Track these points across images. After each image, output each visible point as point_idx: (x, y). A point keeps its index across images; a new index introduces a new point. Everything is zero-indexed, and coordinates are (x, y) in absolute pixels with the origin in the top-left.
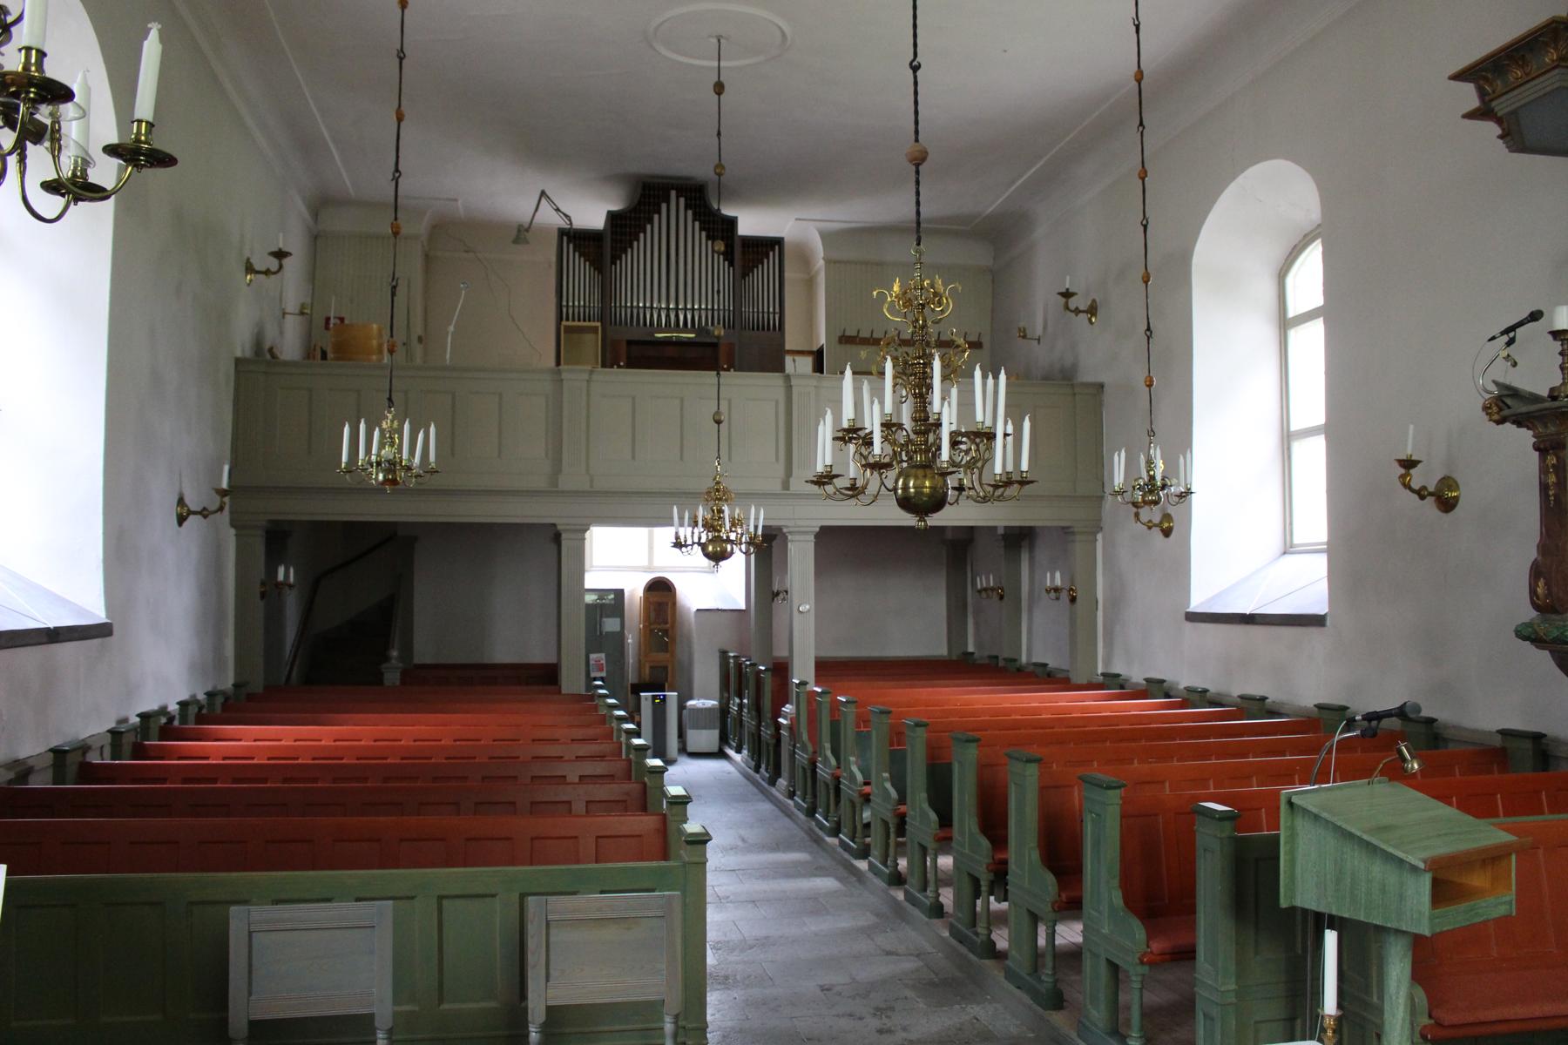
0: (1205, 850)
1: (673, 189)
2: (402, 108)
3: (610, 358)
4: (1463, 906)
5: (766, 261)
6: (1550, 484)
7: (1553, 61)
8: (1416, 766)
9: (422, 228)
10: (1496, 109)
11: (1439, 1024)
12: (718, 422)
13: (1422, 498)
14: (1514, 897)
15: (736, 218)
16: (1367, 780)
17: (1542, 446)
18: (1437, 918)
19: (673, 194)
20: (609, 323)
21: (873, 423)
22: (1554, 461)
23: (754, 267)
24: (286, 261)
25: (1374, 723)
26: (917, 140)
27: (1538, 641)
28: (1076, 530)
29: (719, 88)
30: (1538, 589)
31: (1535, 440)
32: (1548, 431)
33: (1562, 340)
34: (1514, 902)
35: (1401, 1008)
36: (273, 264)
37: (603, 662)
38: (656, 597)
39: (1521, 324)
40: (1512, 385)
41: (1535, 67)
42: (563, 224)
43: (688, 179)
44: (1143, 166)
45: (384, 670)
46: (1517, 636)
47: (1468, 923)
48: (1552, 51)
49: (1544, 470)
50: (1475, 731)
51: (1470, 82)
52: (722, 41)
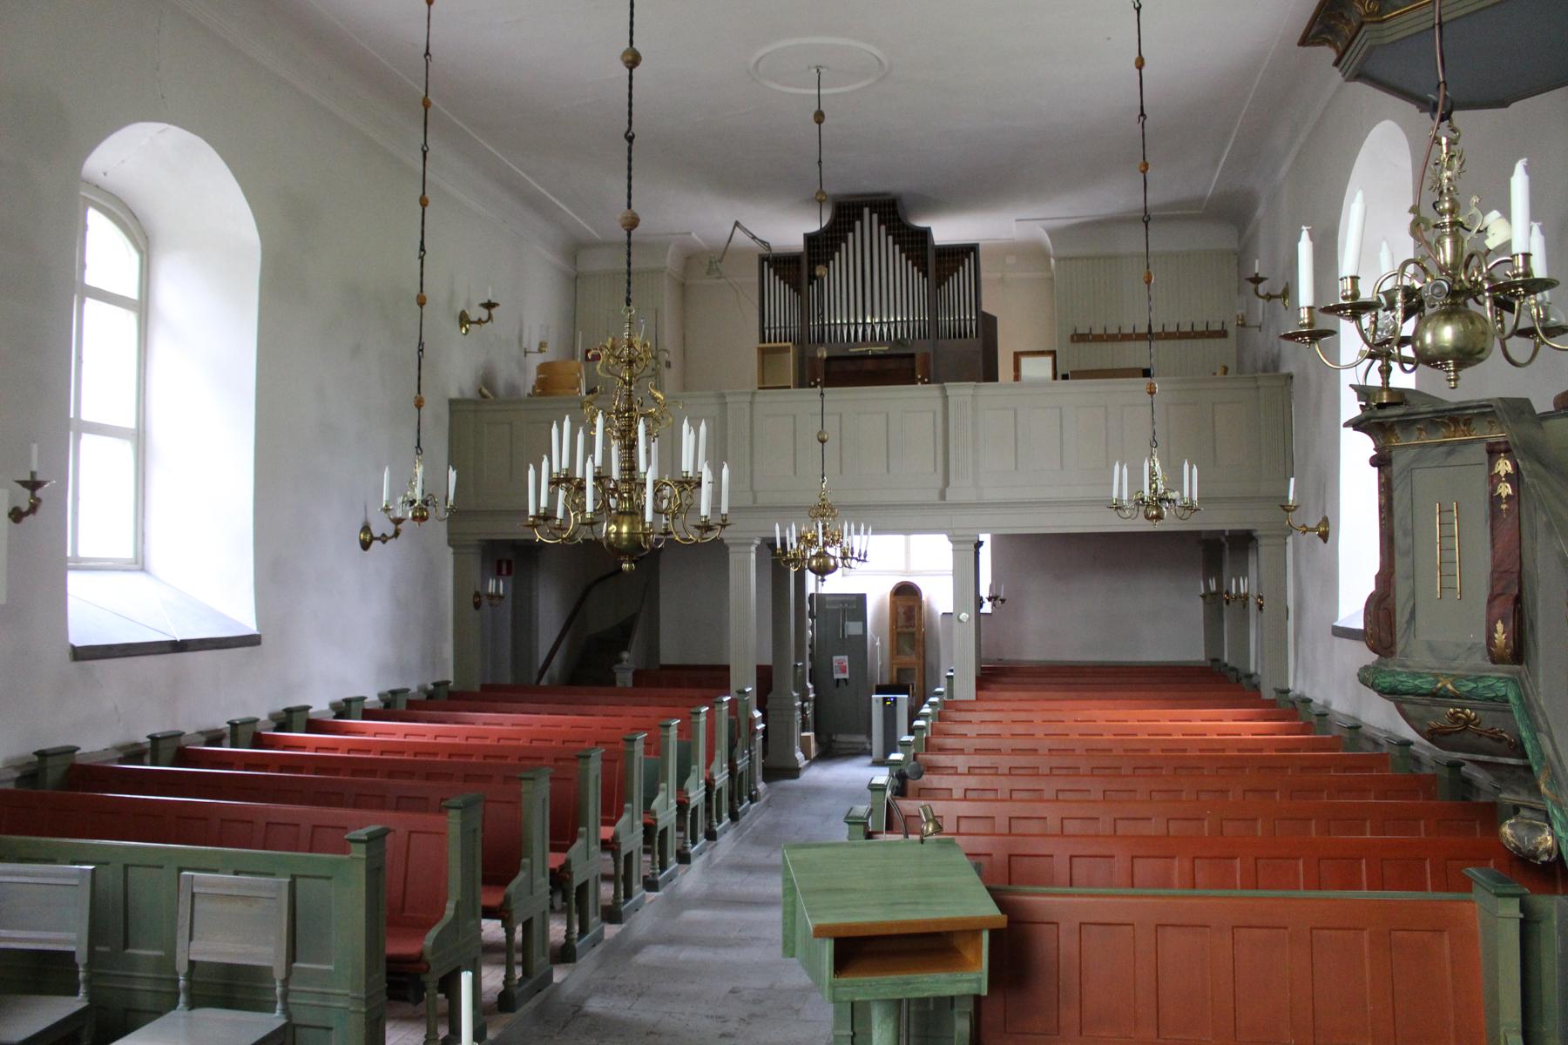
1: (866, 206)
2: (427, 195)
3: (804, 380)
5: (961, 268)
9: (670, 261)
12: (823, 441)
15: (929, 228)
19: (866, 211)
20: (807, 342)
21: (587, 471)
22: (1509, 468)
23: (949, 275)
24: (494, 311)
26: (629, 206)
28: (1258, 533)
29: (819, 117)
36: (484, 314)
37: (846, 664)
38: (903, 602)
42: (764, 252)
43: (884, 194)
44: (1144, 158)
45: (615, 671)
52: (821, 70)
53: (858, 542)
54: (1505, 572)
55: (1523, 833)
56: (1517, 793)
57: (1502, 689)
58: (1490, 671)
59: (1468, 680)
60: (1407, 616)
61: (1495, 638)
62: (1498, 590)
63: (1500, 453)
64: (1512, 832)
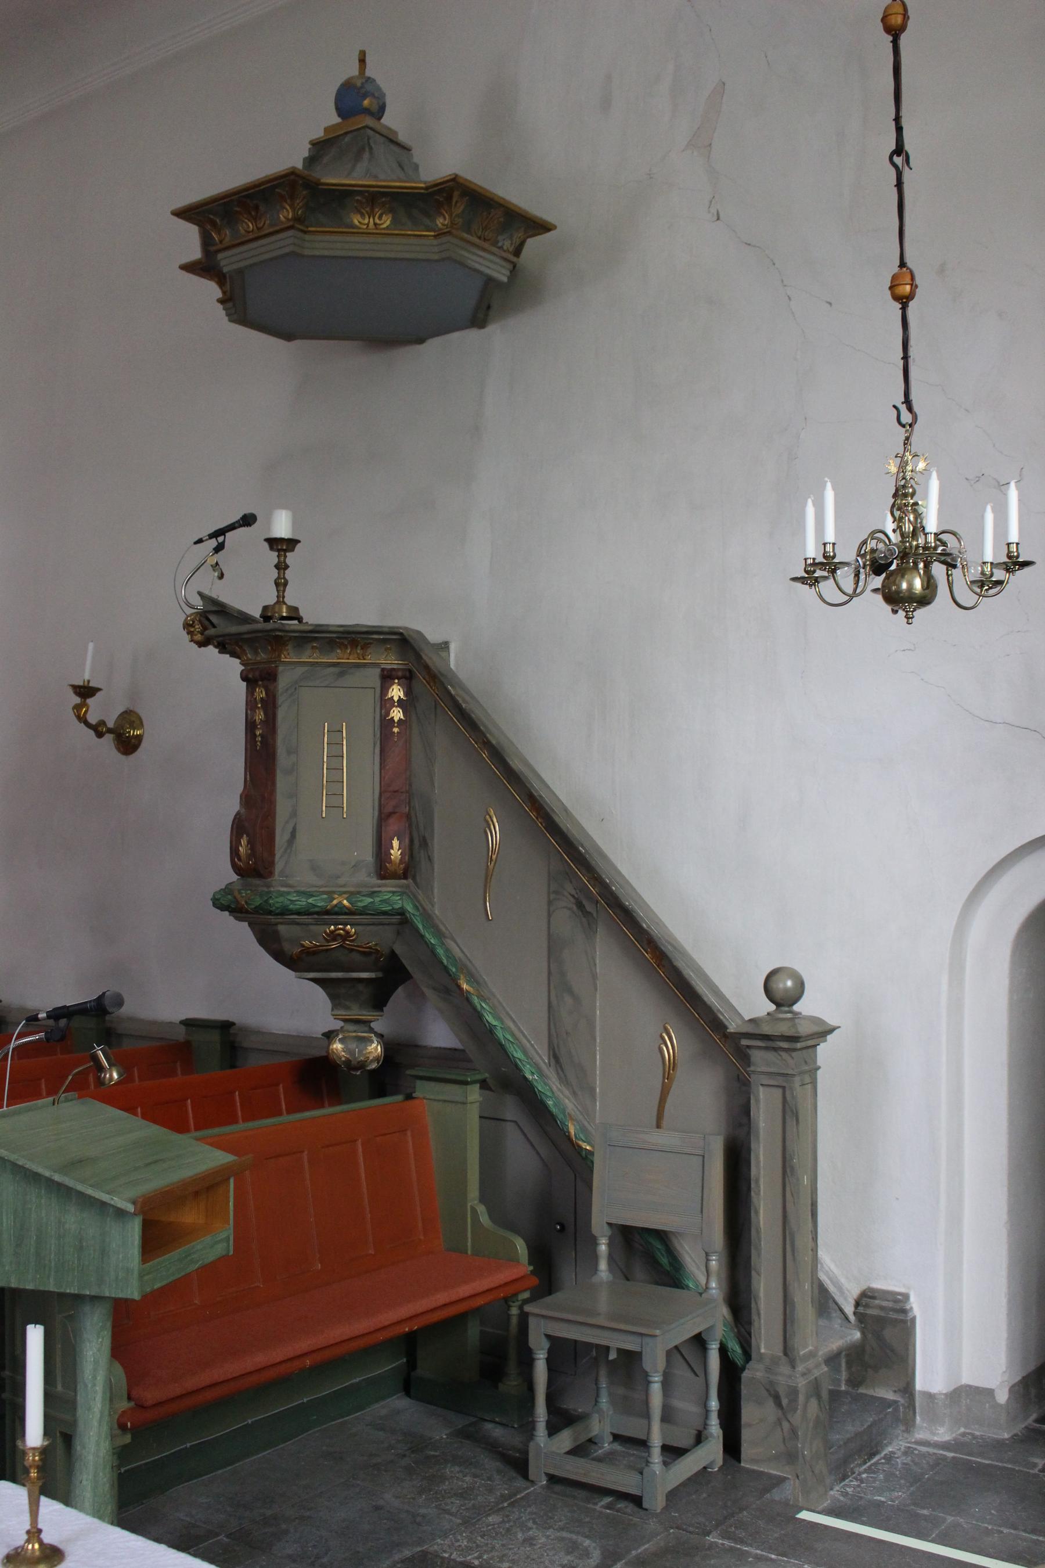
4: (175, 1254)
6: (258, 721)
7: (288, 219)
8: (115, 1076)
10: (222, 263)
11: (140, 1406)
13: (100, 735)
14: (232, 1231)
16: (51, 1099)
17: (250, 676)
18: (148, 1274)
22: (263, 695)
25: (63, 1022)
27: (237, 911)
31: (243, 668)
32: (258, 659)
33: (279, 551)
34: (232, 1238)
35: (99, 1397)
39: (232, 527)
40: (220, 599)
41: (268, 222)
46: (214, 905)
47: (183, 1274)
48: (288, 207)
49: (251, 705)
50: (154, 1023)
51: (195, 224)
54: (395, 792)
55: (353, 1045)
56: (348, 1008)
57: (397, 902)
58: (380, 887)
59: (364, 896)
60: (287, 836)
62: (389, 809)
63: (394, 679)
64: (343, 1046)
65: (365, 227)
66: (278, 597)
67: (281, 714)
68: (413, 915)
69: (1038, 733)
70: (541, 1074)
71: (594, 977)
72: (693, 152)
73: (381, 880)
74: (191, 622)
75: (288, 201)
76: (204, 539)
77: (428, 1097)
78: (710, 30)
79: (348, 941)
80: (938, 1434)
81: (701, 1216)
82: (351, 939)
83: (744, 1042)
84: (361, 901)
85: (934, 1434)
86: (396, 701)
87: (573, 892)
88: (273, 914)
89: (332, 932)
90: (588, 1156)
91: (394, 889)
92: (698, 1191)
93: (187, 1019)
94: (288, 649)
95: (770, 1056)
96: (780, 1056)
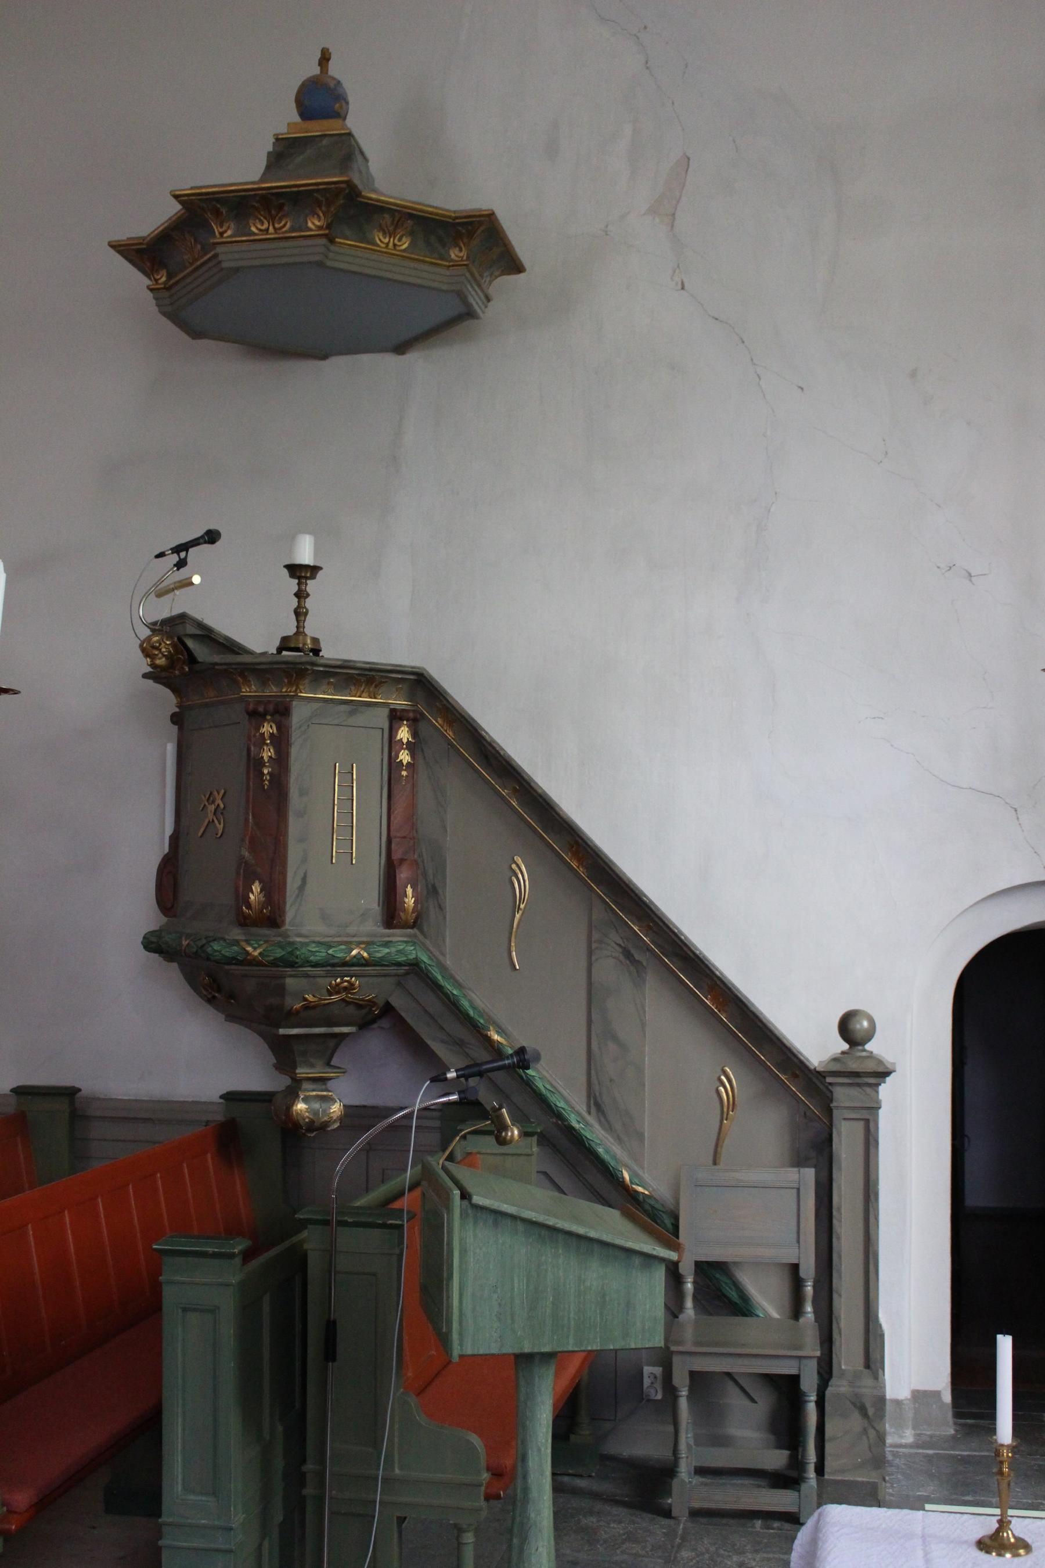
0: (185, 1310)
6: (266, 759)
30: (251, 896)
33: (299, 578)
39: (195, 543)
41: (288, 225)
48: (321, 215)
53: (398, 738)
55: (316, 1106)
58: (389, 936)
61: (405, 903)
63: (403, 720)
65: (383, 245)
66: (298, 627)
67: (294, 751)
68: (429, 965)
69: (1001, 798)
70: (587, 1124)
71: (643, 1025)
72: (654, 218)
73: (389, 929)
74: (157, 645)
75: (324, 208)
76: (167, 553)
77: (483, 1151)
78: (673, 103)
79: (352, 994)
80: (905, 1436)
81: (798, 1245)
82: (354, 991)
83: (829, 1080)
84: (378, 952)
85: (901, 1437)
86: (405, 743)
87: (620, 942)
88: (296, 966)
89: (337, 985)
90: (647, 1200)
91: (405, 939)
92: (794, 1222)
93: (18, 1087)
94: (304, 684)
95: (854, 1092)
96: (864, 1091)
